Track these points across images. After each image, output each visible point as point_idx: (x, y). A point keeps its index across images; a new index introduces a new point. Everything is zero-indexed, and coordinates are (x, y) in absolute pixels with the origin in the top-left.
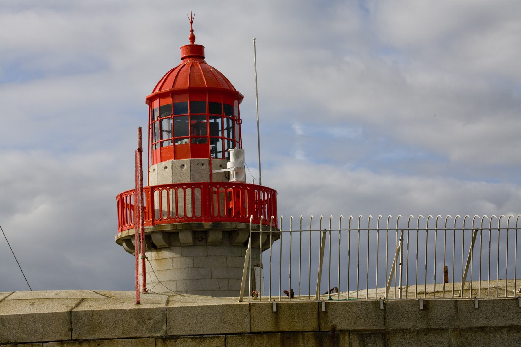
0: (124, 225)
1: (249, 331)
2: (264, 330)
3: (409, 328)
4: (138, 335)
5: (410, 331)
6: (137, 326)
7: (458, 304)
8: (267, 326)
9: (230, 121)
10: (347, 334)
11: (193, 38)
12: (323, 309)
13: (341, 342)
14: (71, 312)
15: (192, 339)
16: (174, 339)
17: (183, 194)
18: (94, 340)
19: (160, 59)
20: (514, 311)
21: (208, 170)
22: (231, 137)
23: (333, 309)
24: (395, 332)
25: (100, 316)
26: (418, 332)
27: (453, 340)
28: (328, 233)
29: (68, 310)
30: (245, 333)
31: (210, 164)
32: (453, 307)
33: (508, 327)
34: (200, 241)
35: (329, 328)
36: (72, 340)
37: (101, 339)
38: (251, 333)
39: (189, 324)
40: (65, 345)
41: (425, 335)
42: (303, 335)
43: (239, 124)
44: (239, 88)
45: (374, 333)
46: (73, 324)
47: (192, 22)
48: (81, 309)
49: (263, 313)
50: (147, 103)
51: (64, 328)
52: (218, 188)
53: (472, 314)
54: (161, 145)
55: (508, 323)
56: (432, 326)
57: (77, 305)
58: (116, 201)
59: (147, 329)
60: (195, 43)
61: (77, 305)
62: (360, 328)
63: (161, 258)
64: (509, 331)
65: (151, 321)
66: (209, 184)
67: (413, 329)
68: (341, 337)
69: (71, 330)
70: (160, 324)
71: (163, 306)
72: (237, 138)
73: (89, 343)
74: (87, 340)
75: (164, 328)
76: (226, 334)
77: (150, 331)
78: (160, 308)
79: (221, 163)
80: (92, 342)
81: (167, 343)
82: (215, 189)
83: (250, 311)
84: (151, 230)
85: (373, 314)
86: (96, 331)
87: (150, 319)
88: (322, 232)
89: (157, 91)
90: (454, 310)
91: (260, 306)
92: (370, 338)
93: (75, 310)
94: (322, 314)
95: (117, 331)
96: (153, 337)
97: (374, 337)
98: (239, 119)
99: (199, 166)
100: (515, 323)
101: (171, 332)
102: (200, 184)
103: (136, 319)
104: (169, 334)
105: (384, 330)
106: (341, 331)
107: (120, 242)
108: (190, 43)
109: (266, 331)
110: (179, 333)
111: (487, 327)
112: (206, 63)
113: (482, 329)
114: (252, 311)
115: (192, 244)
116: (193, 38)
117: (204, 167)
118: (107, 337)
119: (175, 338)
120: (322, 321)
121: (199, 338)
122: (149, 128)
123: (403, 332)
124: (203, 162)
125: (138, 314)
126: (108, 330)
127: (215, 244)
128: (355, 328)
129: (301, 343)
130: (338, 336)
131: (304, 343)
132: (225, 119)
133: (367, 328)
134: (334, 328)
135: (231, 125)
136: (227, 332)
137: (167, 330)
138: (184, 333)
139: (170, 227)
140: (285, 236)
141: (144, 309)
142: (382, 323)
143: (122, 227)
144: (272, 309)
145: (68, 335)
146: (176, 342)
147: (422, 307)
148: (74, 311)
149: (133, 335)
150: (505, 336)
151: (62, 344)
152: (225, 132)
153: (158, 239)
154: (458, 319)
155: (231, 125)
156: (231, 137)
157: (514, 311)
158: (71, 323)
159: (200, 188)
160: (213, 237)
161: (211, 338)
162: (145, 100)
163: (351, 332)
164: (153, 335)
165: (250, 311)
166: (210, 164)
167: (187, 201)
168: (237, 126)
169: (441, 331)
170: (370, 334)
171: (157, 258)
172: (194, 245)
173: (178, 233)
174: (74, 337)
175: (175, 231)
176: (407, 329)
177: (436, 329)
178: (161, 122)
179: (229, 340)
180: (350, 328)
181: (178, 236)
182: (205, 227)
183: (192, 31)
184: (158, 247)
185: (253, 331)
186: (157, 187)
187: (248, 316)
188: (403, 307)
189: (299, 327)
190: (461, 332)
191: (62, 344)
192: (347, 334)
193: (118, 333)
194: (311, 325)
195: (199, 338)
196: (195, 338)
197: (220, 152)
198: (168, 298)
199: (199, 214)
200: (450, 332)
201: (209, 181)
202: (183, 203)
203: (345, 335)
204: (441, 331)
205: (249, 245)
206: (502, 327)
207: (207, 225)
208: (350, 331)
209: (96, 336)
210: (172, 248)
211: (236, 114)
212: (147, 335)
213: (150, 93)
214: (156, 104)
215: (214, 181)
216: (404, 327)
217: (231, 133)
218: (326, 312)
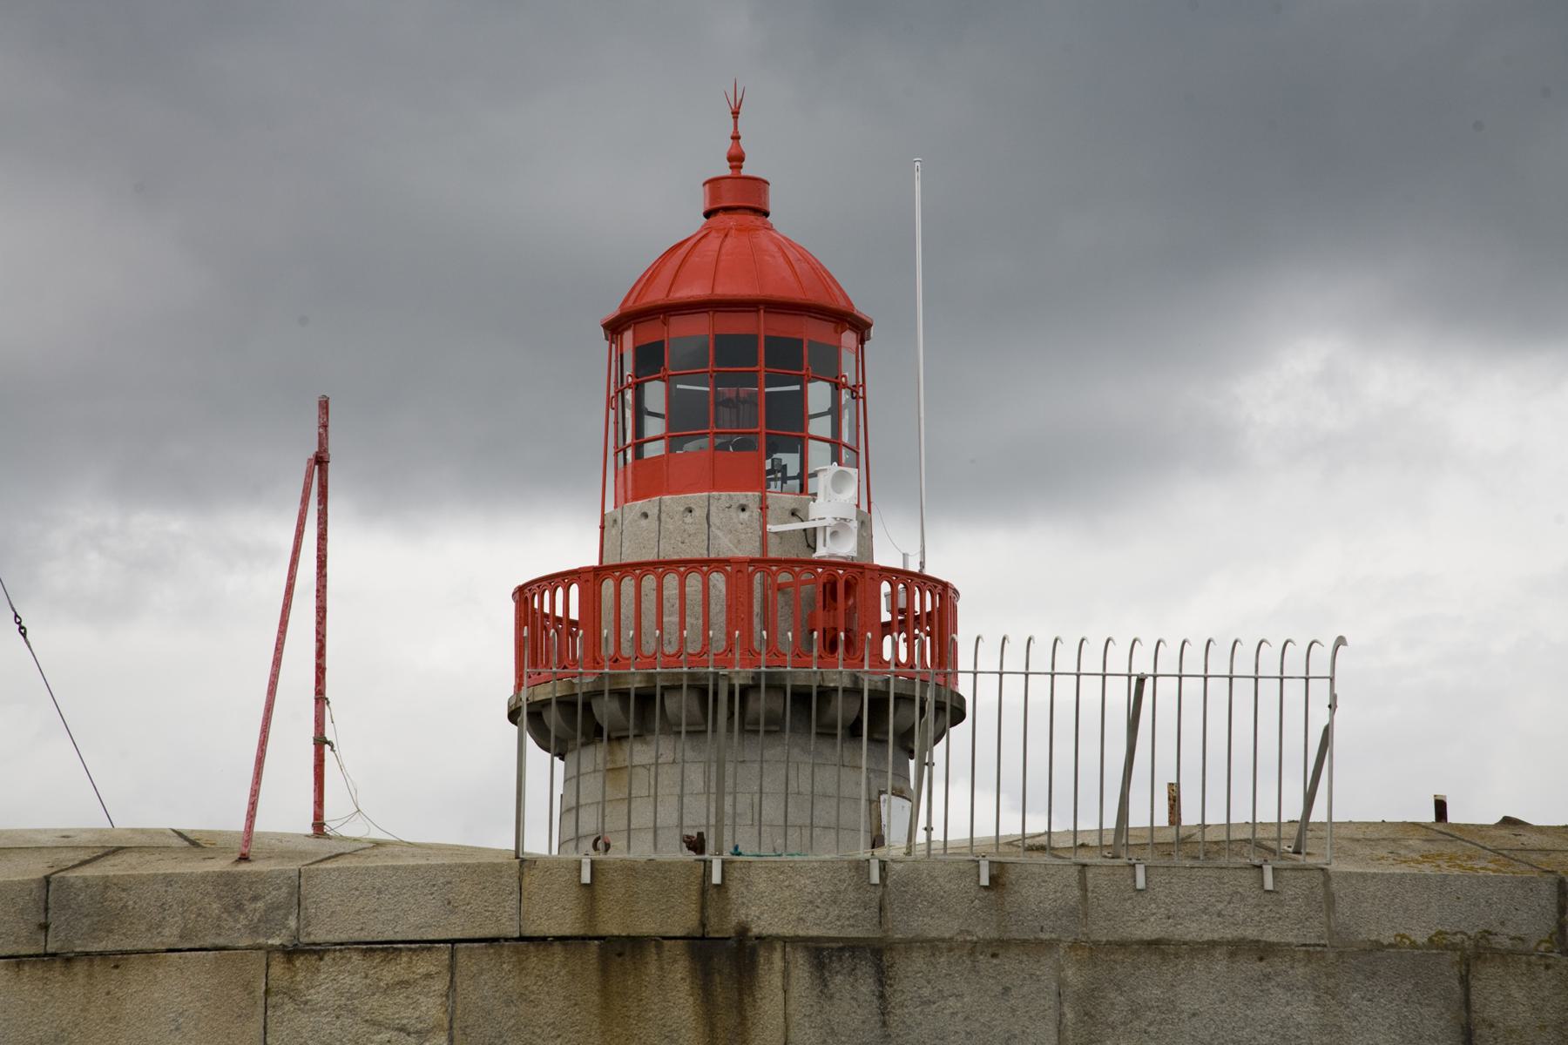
1: (517, 935)
2: (555, 930)
3: (947, 935)
4: (221, 941)
5: (950, 945)
6: (219, 918)
7: (1090, 875)
8: (561, 919)
10: (778, 945)
11: (736, 159)
13: (762, 969)
15: (365, 952)
16: (315, 952)
18: (103, 954)
19: (648, 213)
20: (1251, 901)
21: (757, 525)
23: (743, 880)
24: (910, 944)
26: (974, 948)
27: (1070, 973)
28: (1149, 682)
30: (506, 940)
31: (764, 508)
32: (1074, 884)
33: (1229, 943)
35: (729, 929)
36: (46, 955)
37: (122, 953)
38: (522, 938)
39: (358, 913)
40: (27, 968)
41: (994, 956)
42: (659, 947)
45: (851, 948)
46: (51, 913)
47: (736, 114)
49: (556, 887)
51: (25, 921)
53: (1128, 905)
54: (638, 454)
55: (1229, 934)
56: (1015, 934)
59: (245, 926)
60: (745, 172)
62: (814, 932)
64: (1232, 955)
65: (260, 904)
67: (960, 938)
68: (762, 953)
69: (45, 927)
70: (282, 912)
73: (91, 961)
74: (87, 954)
75: (292, 923)
76: (453, 942)
77: (254, 930)
79: (794, 506)
80: (97, 961)
81: (298, 964)
83: (520, 880)
85: (852, 895)
86: (111, 931)
87: (255, 899)
88: (1134, 679)
89: (630, 303)
90: (1077, 892)
92: (840, 959)
94: (712, 892)
95: (167, 932)
96: (260, 948)
97: (853, 957)
99: (733, 513)
100: (1251, 933)
101: (309, 934)
102: (727, 561)
103: (220, 897)
104: (304, 939)
105: (880, 939)
106: (758, 938)
109: (560, 933)
110: (330, 938)
111: (1168, 942)
113: (1154, 945)
114: (527, 880)
116: (736, 159)
117: (744, 516)
118: (139, 947)
119: (317, 951)
120: (711, 912)
121: (382, 950)
123: (933, 946)
124: (743, 501)
125: (226, 885)
126: (143, 928)
127: (774, 727)
128: (801, 933)
129: (653, 969)
130: (753, 952)
131: (662, 968)
133: (833, 933)
134: (743, 931)
136: (458, 936)
137: (298, 929)
138: (344, 937)
139: (638, 678)
142: (875, 921)
145: (37, 942)
146: (321, 959)
147: (985, 881)
149: (208, 942)
150: (1220, 967)
151: (18, 965)
153: (606, 710)
154: (1086, 915)
156: (845, 438)
157: (1251, 901)
158: (46, 909)
161: (414, 950)
163: (795, 941)
164: (261, 940)
165: (520, 880)
166: (764, 508)
169: (1037, 946)
170: (841, 949)
171: (609, 766)
174: (50, 949)
176: (943, 940)
177: (1025, 941)
178: (638, 390)
179: (462, 958)
180: (788, 931)
183: (736, 138)
185: (527, 933)
187: (516, 896)
188: (934, 879)
189: (647, 927)
190: (1096, 951)
191: (18, 965)
192: (778, 945)
193: (170, 936)
194: (683, 920)
195: (382, 950)
196: (372, 950)
197: (793, 478)
200: (1062, 952)
203: (772, 949)
204: (1037, 946)
206: (1213, 944)
208: (785, 940)
209: (108, 945)
210: (649, 738)
212: (244, 942)
213: (612, 310)
214: (628, 336)
215: (772, 555)
216: (934, 934)
218: (721, 887)
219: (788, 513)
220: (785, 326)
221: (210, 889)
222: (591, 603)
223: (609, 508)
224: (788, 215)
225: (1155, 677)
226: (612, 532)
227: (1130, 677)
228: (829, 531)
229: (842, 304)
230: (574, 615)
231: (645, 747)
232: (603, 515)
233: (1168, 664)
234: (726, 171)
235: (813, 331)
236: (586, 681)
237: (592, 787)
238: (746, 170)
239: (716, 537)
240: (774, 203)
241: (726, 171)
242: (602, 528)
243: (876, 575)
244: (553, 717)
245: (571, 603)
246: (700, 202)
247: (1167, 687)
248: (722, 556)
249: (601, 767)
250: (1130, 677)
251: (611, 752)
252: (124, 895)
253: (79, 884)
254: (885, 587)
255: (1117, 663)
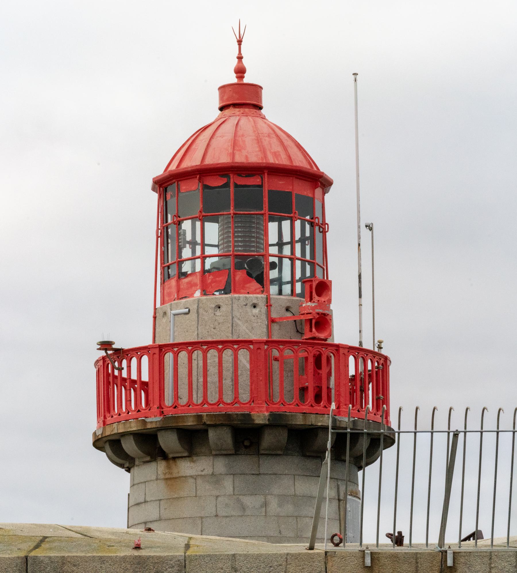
0: (109, 411)
9: (308, 227)
11: (240, 72)
12: (450, 563)
14: (26, 558)
17: (217, 360)
22: (308, 257)
25: (75, 566)
28: (461, 436)
29: (22, 554)
34: (246, 447)
43: (324, 232)
44: (325, 166)
47: (240, 42)
48: (38, 553)
49: (349, 568)
50: (154, 189)
52: (281, 351)
57: (37, 547)
58: (94, 371)
60: (246, 80)
61: (37, 547)
63: (175, 475)
66: (267, 342)
71: (180, 553)
72: (319, 260)
78: (173, 557)
79: (288, 304)
82: (275, 353)
84: (158, 425)
88: (451, 434)
91: (343, 557)
93: (33, 554)
98: (324, 223)
99: (249, 309)
102: (251, 342)
107: (100, 444)
108: (235, 80)
112: (264, 118)
114: (329, 565)
115: (233, 452)
116: (240, 72)
117: (256, 311)
122: (158, 237)
124: (255, 301)
125: (139, 563)
127: (273, 453)
132: (298, 223)
135: (308, 234)
140: (405, 441)
141: (149, 558)
143: (105, 417)
144: (364, 562)
148: (31, 557)
152: (298, 246)
155: (308, 234)
159: (249, 349)
160: (268, 439)
162: (150, 183)
167: (224, 372)
168: (318, 236)
171: (167, 476)
172: (236, 454)
173: (206, 431)
175: (199, 427)
181: (207, 435)
182: (257, 422)
183: (240, 58)
184: (171, 456)
186: (170, 347)
198: (188, 542)
199: (245, 396)
201: (265, 338)
202: (217, 376)
205: (328, 454)
207: (261, 417)
210: (195, 458)
211: (318, 213)
213: (159, 171)
215: (275, 338)
217: (308, 248)
219: (284, 309)
220: (281, 184)
221: (129, 566)
222: (157, 369)
223: (158, 305)
224: (272, 110)
225: (465, 433)
226: (162, 321)
227: (449, 433)
228: (314, 321)
229: (299, 162)
230: (145, 377)
231: (192, 464)
232: (155, 309)
233: (474, 424)
234: (233, 79)
235: (299, 189)
236: (154, 420)
237: (157, 490)
238: (247, 79)
239: (237, 325)
240: (266, 101)
241: (233, 79)
242: (155, 318)
243: (346, 351)
244: (129, 446)
245: (142, 369)
246: (217, 103)
247: (473, 439)
248: (241, 339)
249: (162, 476)
250: (449, 433)
251: (169, 467)
252: (75, 568)
253: (47, 561)
254: (351, 360)
255: (441, 424)
